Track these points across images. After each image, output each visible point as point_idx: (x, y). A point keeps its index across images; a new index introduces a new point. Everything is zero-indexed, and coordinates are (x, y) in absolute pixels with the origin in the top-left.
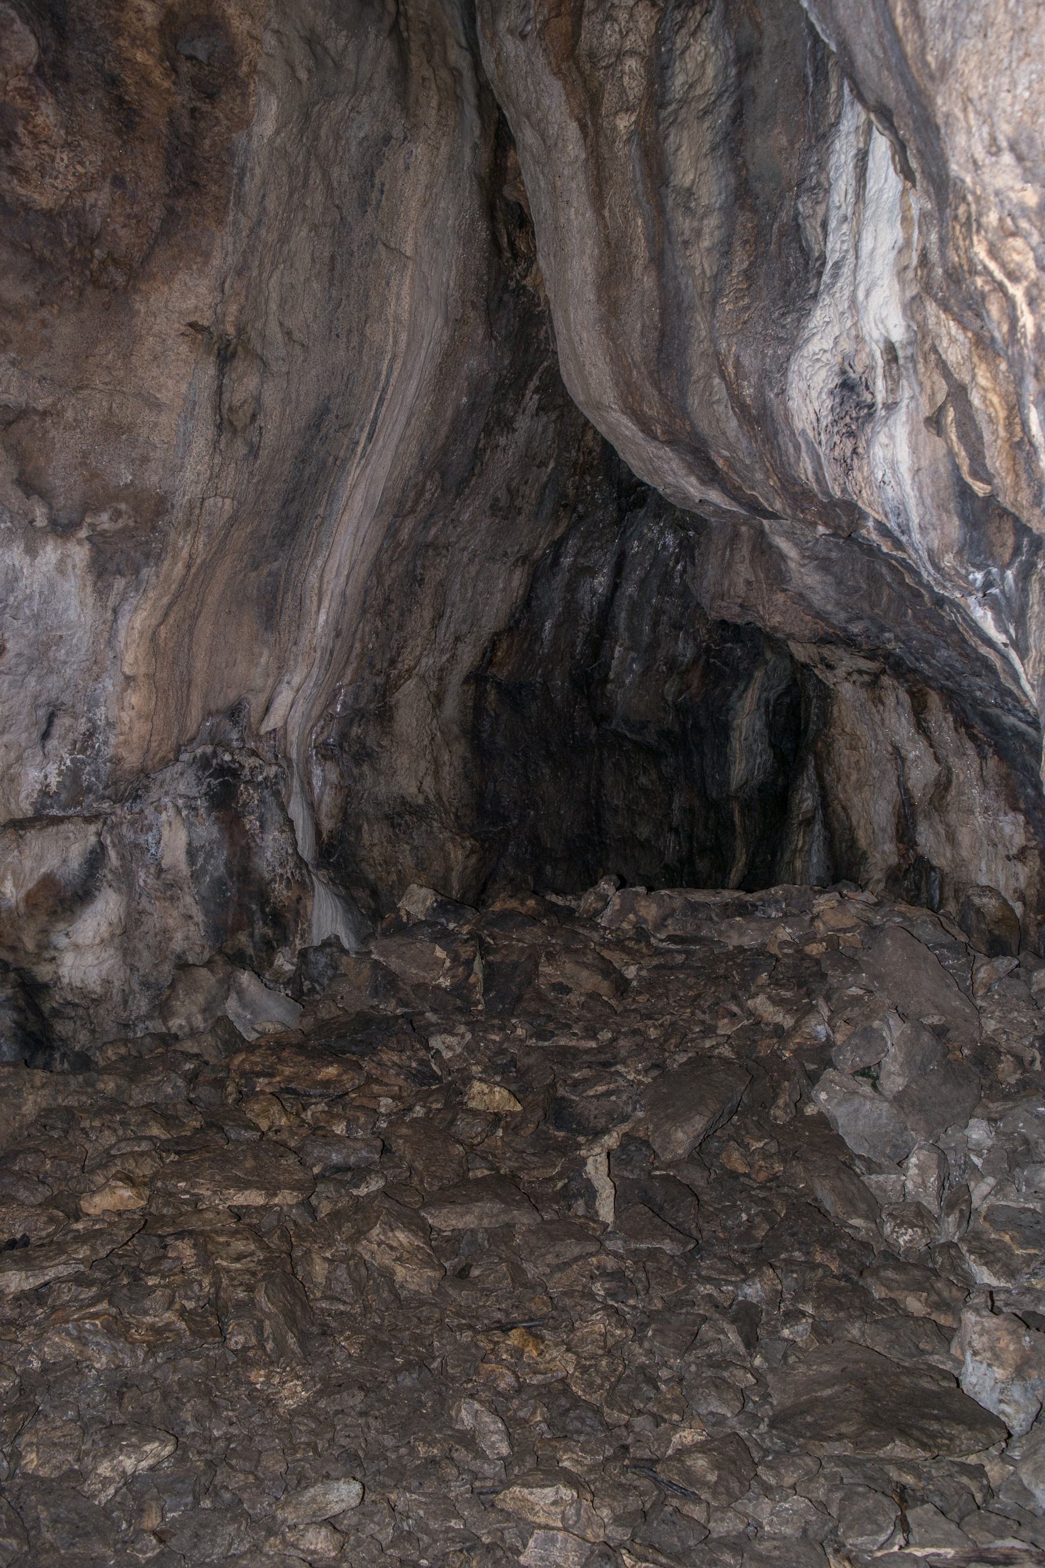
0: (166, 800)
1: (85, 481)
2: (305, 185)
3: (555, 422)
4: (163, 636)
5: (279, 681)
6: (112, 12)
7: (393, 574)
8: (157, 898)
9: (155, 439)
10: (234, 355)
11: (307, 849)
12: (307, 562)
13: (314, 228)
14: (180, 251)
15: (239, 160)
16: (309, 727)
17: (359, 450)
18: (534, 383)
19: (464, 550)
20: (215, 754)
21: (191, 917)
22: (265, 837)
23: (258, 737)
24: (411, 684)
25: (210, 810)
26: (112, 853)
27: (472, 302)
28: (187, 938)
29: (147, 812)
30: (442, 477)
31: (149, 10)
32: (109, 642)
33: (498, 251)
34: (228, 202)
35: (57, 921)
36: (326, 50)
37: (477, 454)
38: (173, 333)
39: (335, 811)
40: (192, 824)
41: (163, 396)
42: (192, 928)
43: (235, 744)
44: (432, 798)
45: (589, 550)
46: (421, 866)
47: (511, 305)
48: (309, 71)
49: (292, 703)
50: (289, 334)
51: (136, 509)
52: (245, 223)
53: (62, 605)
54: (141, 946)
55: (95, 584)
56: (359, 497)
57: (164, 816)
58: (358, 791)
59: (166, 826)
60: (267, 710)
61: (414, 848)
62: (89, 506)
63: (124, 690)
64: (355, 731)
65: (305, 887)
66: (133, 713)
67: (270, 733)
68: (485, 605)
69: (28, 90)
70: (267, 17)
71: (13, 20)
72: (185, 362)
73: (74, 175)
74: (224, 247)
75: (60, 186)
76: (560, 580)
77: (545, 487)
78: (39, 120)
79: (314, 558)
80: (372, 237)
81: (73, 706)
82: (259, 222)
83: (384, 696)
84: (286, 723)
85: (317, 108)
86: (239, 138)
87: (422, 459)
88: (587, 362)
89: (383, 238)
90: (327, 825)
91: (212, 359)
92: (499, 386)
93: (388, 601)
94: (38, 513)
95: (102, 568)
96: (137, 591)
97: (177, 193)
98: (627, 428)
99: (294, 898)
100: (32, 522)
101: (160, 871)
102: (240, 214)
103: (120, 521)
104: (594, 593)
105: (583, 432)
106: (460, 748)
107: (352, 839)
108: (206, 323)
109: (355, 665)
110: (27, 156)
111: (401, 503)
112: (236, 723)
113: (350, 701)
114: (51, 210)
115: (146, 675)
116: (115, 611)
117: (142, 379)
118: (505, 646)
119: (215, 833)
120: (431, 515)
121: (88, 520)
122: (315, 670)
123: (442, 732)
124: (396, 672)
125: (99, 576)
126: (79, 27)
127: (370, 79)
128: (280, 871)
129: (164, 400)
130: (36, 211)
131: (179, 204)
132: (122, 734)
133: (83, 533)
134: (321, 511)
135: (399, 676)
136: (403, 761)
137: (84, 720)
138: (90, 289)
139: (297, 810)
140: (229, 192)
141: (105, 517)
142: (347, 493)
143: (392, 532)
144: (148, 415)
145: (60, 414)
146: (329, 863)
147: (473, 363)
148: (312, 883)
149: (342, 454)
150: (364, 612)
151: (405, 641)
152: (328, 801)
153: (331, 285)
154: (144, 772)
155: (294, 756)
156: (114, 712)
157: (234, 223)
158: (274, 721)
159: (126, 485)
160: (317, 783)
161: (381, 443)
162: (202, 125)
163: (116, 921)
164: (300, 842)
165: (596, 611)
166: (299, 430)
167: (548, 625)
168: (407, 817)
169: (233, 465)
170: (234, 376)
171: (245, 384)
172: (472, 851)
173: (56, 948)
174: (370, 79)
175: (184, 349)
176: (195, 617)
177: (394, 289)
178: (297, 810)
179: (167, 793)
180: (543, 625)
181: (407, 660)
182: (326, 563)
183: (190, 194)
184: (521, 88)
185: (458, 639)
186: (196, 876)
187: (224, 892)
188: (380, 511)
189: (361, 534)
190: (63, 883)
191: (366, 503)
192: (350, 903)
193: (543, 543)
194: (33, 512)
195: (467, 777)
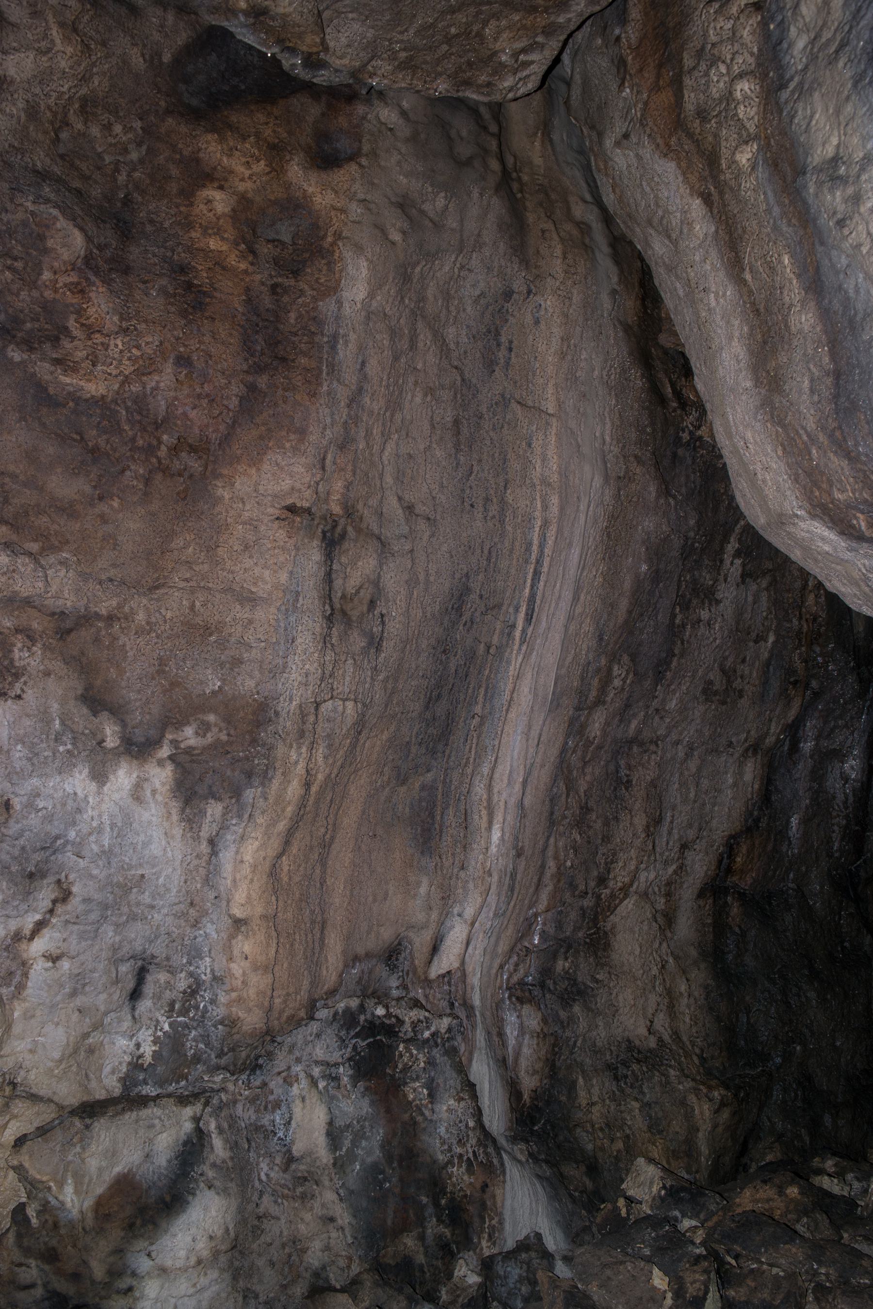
0: (297, 1069)
1: (164, 692)
2: (413, 346)
3: (767, 589)
4: (286, 869)
5: (445, 914)
6: (182, 209)
7: (588, 778)
8: (284, 1197)
9: (249, 637)
10: (343, 535)
11: (496, 1119)
12: (469, 771)
13: (429, 391)
14: (269, 430)
15: (329, 329)
16: (496, 965)
17: (518, 634)
18: (732, 546)
19: (677, 743)
20: (362, 1008)
21: (332, 1220)
22: (437, 1107)
23: (427, 982)
24: (629, 904)
25: (355, 1080)
26: (217, 1142)
27: (636, 457)
28: (327, 1248)
29: (272, 1085)
30: (632, 660)
31: (218, 198)
32: (206, 880)
33: (662, 401)
34: (321, 371)
35: (135, 1237)
36: (422, 212)
37: (674, 632)
38: (266, 519)
39: (538, 1066)
40: (332, 1098)
41: (261, 590)
42: (334, 1234)
43: (395, 993)
44: (666, 1038)
45: (832, 731)
46: (655, 1127)
47: (689, 461)
48: (404, 233)
49: (469, 938)
50: (409, 509)
51: (228, 720)
52: (343, 394)
53: (142, 838)
54: (261, 1262)
55: (183, 811)
56: (526, 690)
57: (295, 1090)
58: (568, 1039)
59: (298, 1102)
60: (435, 949)
61: (646, 1106)
62: (171, 720)
63: (231, 937)
64: (561, 965)
65: (490, 1171)
66: (246, 964)
67: (443, 976)
68: (714, 805)
69: (78, 283)
70: (353, 190)
71: (55, 217)
72: (283, 549)
73: (129, 359)
74: (323, 420)
75: (114, 373)
76: (802, 769)
77: (768, 664)
78: (91, 311)
79: (477, 765)
80: (503, 396)
81: (168, 959)
82: (360, 390)
83: (595, 921)
84: (463, 963)
85: (418, 270)
86: (327, 307)
87: (601, 639)
88: (758, 467)
89: (517, 397)
90: (528, 1083)
91: (316, 543)
92: (687, 552)
93: (586, 809)
94: (108, 731)
95: (190, 791)
96: (240, 817)
97: (259, 369)
98: (823, 539)
99: (478, 1186)
100: (100, 743)
101: (290, 1159)
102: (335, 383)
103: (209, 735)
104: (846, 779)
105: (803, 597)
106: (700, 975)
107: (563, 1098)
108: (306, 505)
109: (550, 888)
110: (77, 349)
111: (582, 694)
112: (393, 968)
113: (551, 930)
114: (103, 397)
115: (264, 917)
116: (212, 842)
117: (233, 572)
118: (744, 849)
119: (365, 1107)
120: (628, 706)
121: (169, 736)
122: (492, 899)
123: (676, 958)
124: (608, 891)
125: (187, 802)
126: (149, 228)
127: (479, 235)
128: (459, 1150)
129: (260, 594)
130: (87, 400)
131: (262, 381)
132: (232, 990)
133: (165, 751)
134: (478, 709)
135: (612, 896)
136: (625, 997)
137: (183, 975)
138: (159, 477)
139: (482, 1071)
140: (321, 362)
141: (189, 731)
142: (510, 686)
143: (576, 728)
144: (241, 612)
145: (128, 618)
146: (532, 1132)
147: (649, 524)
148: (502, 1164)
149: (495, 640)
150: (552, 822)
151: (614, 854)
152: (528, 1055)
153: (458, 450)
154: (269, 1036)
155: (477, 1002)
156: (221, 962)
157: (329, 394)
158: (447, 961)
159: (213, 692)
160: (511, 1033)
161: (544, 624)
162: (286, 299)
163: (219, 1233)
164: (486, 1112)
165: (851, 799)
166: (433, 615)
167: (794, 821)
168: (635, 1067)
169: (350, 661)
170: (344, 559)
171: (359, 567)
172: (723, 1104)
173: (134, 1274)
174: (479, 235)
175: (281, 534)
176: (326, 845)
177: (538, 450)
178: (482, 1071)
179: (298, 1060)
180: (788, 822)
181: (620, 876)
182: (493, 770)
183: (276, 369)
184: (639, 196)
185: (684, 847)
186: (340, 1165)
187: (381, 1184)
188: (555, 704)
189: (534, 733)
190: (145, 1186)
191: (536, 695)
192: (556, 1185)
193: (774, 728)
194: (102, 731)
195: (711, 1009)
